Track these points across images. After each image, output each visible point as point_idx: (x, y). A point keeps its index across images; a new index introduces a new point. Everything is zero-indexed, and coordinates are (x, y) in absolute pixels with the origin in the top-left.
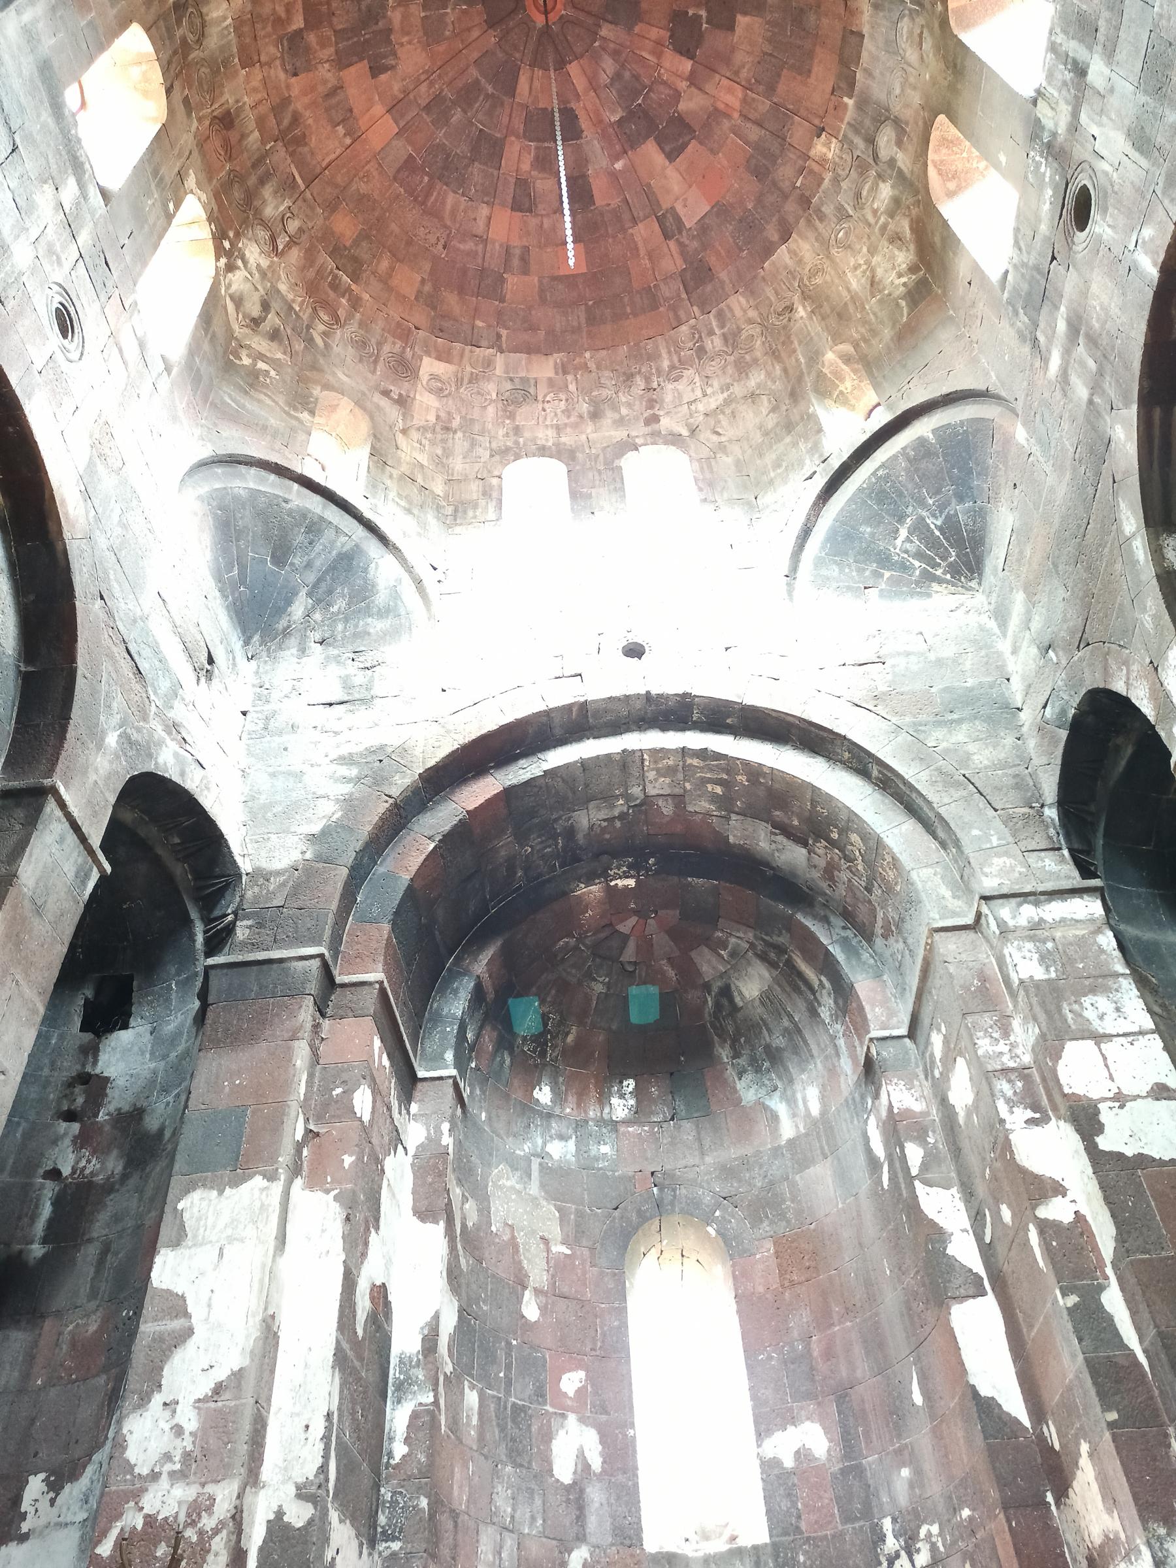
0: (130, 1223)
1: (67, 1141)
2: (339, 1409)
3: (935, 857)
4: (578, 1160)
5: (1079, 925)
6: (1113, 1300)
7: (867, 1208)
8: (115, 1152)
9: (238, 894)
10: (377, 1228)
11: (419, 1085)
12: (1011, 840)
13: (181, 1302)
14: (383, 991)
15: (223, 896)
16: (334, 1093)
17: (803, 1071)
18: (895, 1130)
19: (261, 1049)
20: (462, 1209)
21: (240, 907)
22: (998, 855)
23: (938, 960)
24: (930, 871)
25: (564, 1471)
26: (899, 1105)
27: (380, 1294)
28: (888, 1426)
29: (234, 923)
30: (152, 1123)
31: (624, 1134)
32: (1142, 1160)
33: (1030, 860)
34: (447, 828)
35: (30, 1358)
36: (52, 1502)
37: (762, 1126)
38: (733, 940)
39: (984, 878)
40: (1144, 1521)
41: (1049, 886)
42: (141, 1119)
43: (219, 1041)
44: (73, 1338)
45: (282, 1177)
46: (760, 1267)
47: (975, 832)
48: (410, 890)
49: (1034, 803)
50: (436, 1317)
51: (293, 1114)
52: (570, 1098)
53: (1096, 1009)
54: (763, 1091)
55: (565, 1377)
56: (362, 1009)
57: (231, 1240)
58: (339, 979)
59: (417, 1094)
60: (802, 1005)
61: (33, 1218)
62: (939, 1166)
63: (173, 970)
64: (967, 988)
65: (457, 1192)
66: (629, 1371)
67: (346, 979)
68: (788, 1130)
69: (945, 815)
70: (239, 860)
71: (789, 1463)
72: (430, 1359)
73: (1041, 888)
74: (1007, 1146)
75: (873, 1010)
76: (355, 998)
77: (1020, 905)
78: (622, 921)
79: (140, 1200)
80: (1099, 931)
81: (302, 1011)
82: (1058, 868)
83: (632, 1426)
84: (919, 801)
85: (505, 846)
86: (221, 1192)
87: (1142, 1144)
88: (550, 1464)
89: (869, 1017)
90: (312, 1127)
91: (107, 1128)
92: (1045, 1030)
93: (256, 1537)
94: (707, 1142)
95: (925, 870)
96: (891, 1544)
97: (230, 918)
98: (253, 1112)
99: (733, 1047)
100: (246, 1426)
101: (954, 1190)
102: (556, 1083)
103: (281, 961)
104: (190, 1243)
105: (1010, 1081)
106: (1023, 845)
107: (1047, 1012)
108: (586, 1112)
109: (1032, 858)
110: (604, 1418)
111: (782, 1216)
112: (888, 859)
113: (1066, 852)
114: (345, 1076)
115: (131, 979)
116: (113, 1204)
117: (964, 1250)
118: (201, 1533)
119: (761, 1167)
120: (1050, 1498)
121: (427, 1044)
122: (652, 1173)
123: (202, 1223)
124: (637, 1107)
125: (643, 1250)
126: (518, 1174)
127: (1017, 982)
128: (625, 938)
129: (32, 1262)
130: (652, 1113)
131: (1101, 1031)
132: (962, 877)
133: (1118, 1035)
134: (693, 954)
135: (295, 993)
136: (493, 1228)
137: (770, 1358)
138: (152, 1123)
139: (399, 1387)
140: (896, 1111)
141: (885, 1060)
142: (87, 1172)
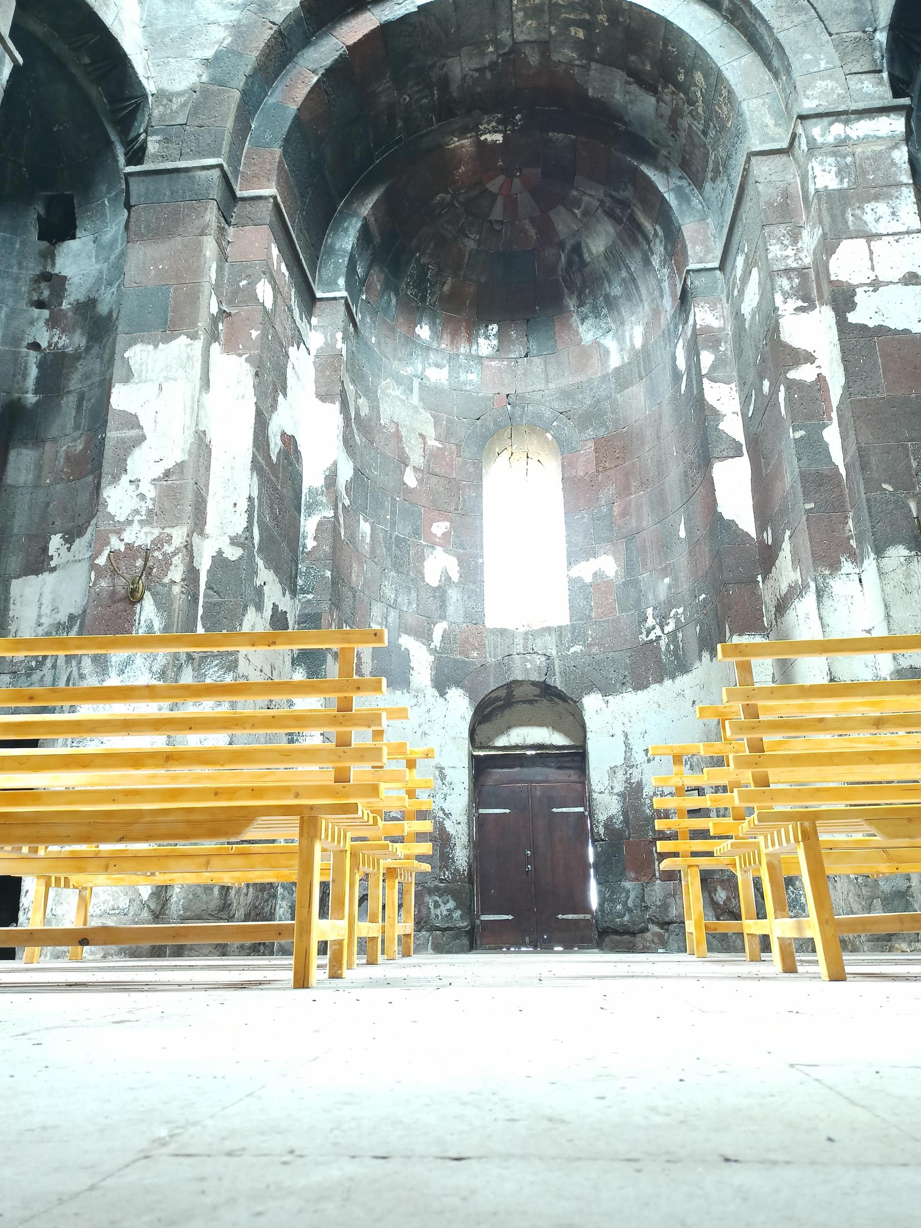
0: (96, 379)
1: (41, 323)
2: (259, 498)
3: (766, 88)
4: (450, 383)
5: (879, 142)
6: (832, 435)
7: (667, 410)
8: (79, 331)
9: (147, 114)
10: (285, 395)
11: (318, 304)
12: (838, 63)
13: (134, 419)
14: (276, 205)
15: (135, 119)
16: (241, 284)
17: (633, 313)
18: (696, 342)
19: (177, 242)
20: (355, 401)
21: (149, 125)
22: (822, 78)
23: (751, 181)
24: (760, 101)
25: (432, 577)
26: (701, 323)
27: (289, 441)
28: (659, 554)
29: (145, 141)
30: (103, 309)
31: (487, 367)
32: (881, 330)
33: (850, 83)
34: (329, 62)
35: (39, 467)
36: (69, 549)
37: (595, 360)
38: (586, 198)
39: (804, 100)
40: (815, 566)
41: (861, 105)
42: (95, 307)
43: (142, 235)
44: (67, 454)
45: (202, 337)
46: (582, 459)
47: (808, 57)
48: (297, 118)
49: (867, 30)
50: (335, 464)
51: (207, 292)
52: (445, 337)
53: (876, 215)
54: (600, 333)
55: (435, 525)
56: (260, 219)
57: (167, 379)
58: (239, 194)
59: (316, 311)
60: (638, 256)
61: (25, 376)
62: (725, 368)
63: (104, 189)
64: (769, 204)
65: (350, 388)
66: (481, 525)
67: (245, 194)
68: (615, 361)
69: (782, 40)
70: (144, 82)
71: (588, 579)
72: (331, 490)
73: (854, 107)
74: (776, 329)
75: (693, 247)
76: (254, 210)
77: (831, 123)
78: (492, 179)
79: (102, 362)
80: (896, 146)
81: (208, 212)
82: (876, 89)
83: (482, 556)
84: (762, 30)
85: (385, 91)
86: (156, 346)
87: (883, 318)
88: (422, 574)
89: (689, 253)
90: (224, 308)
91: (70, 314)
92: (827, 230)
93: (204, 565)
94: (552, 372)
95: (755, 101)
96: (651, 622)
97: (142, 137)
98: (175, 290)
99: (579, 298)
100: (190, 496)
101: (733, 385)
102: (434, 324)
103: (187, 170)
104: (137, 381)
105: (790, 279)
106: (848, 68)
107: (833, 217)
108: (457, 348)
109: (853, 81)
110: (461, 551)
111: (604, 424)
112: (725, 93)
113: (885, 75)
114: (248, 272)
115: (71, 198)
116: (82, 368)
117: (733, 427)
118: (164, 554)
119: (591, 389)
120: (759, 578)
121: (324, 272)
122: (508, 395)
123: (144, 367)
124: (499, 346)
125: (497, 450)
126: (402, 388)
127: (813, 192)
128: (494, 197)
129: (29, 406)
130: (510, 351)
131: (874, 231)
132: (786, 107)
133: (888, 235)
134: (551, 214)
135: (201, 198)
136: (382, 422)
137: (583, 517)
138: (103, 309)
139: (309, 507)
140: (698, 327)
141: (696, 288)
142: (60, 345)
